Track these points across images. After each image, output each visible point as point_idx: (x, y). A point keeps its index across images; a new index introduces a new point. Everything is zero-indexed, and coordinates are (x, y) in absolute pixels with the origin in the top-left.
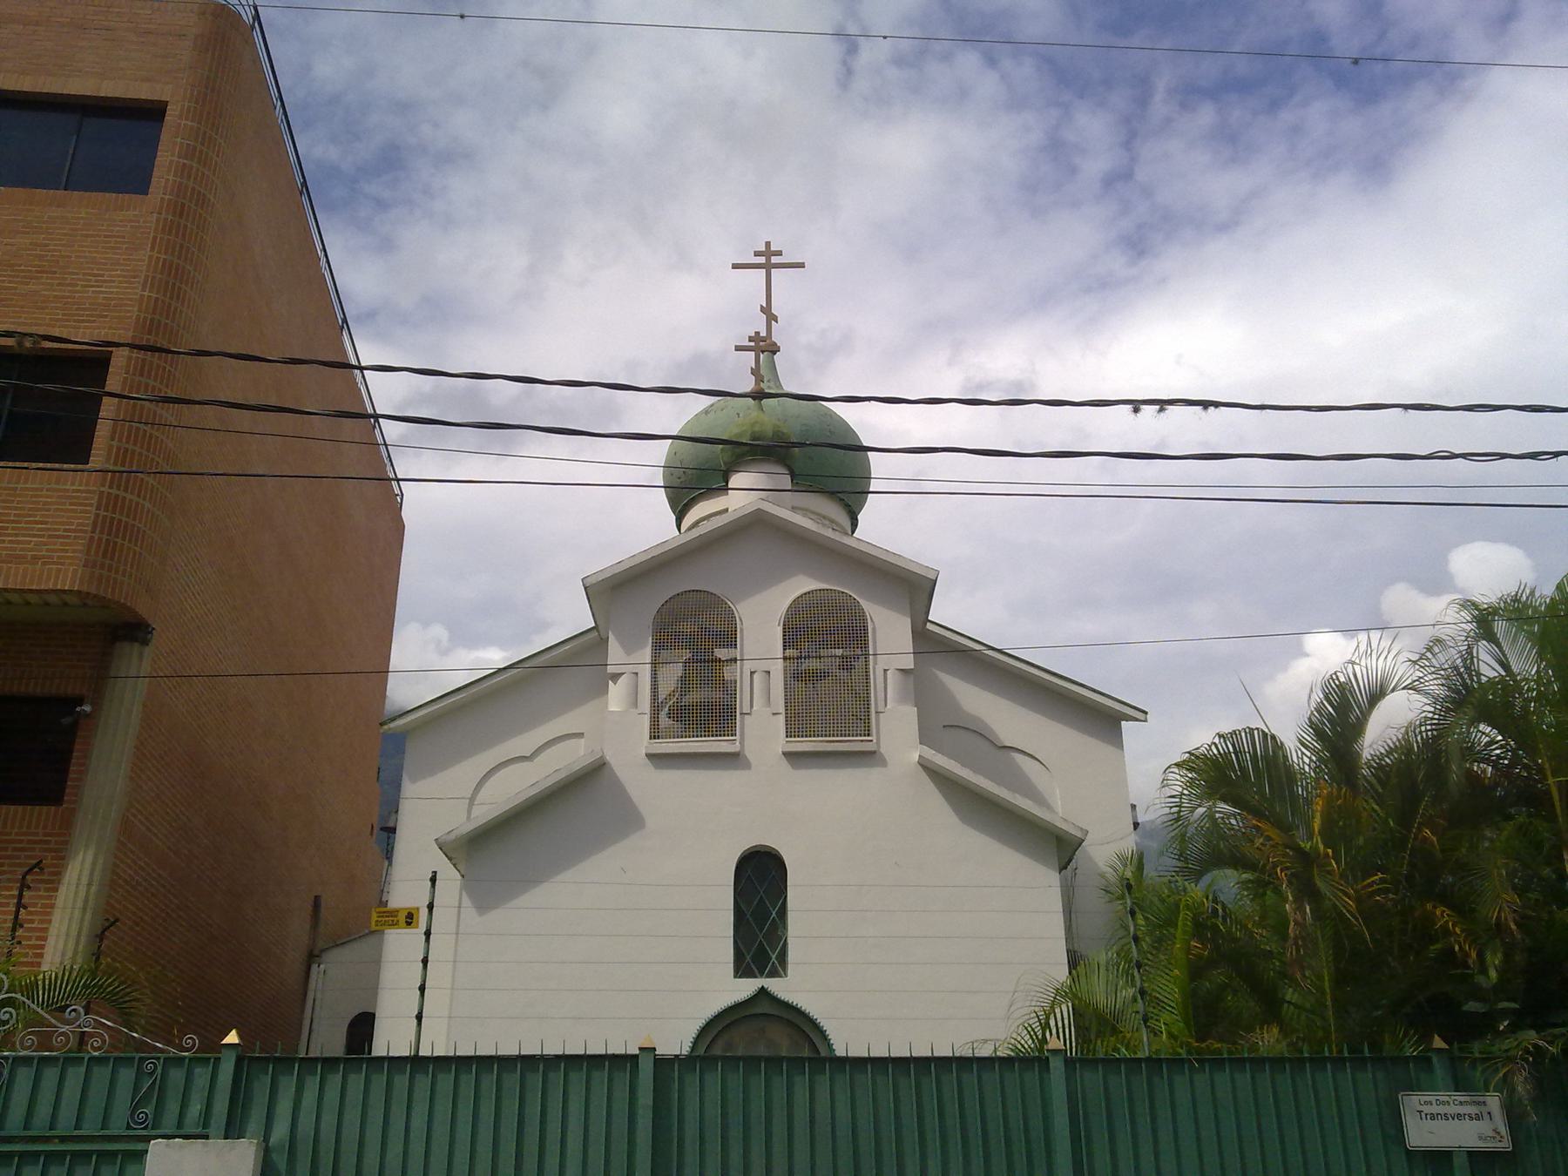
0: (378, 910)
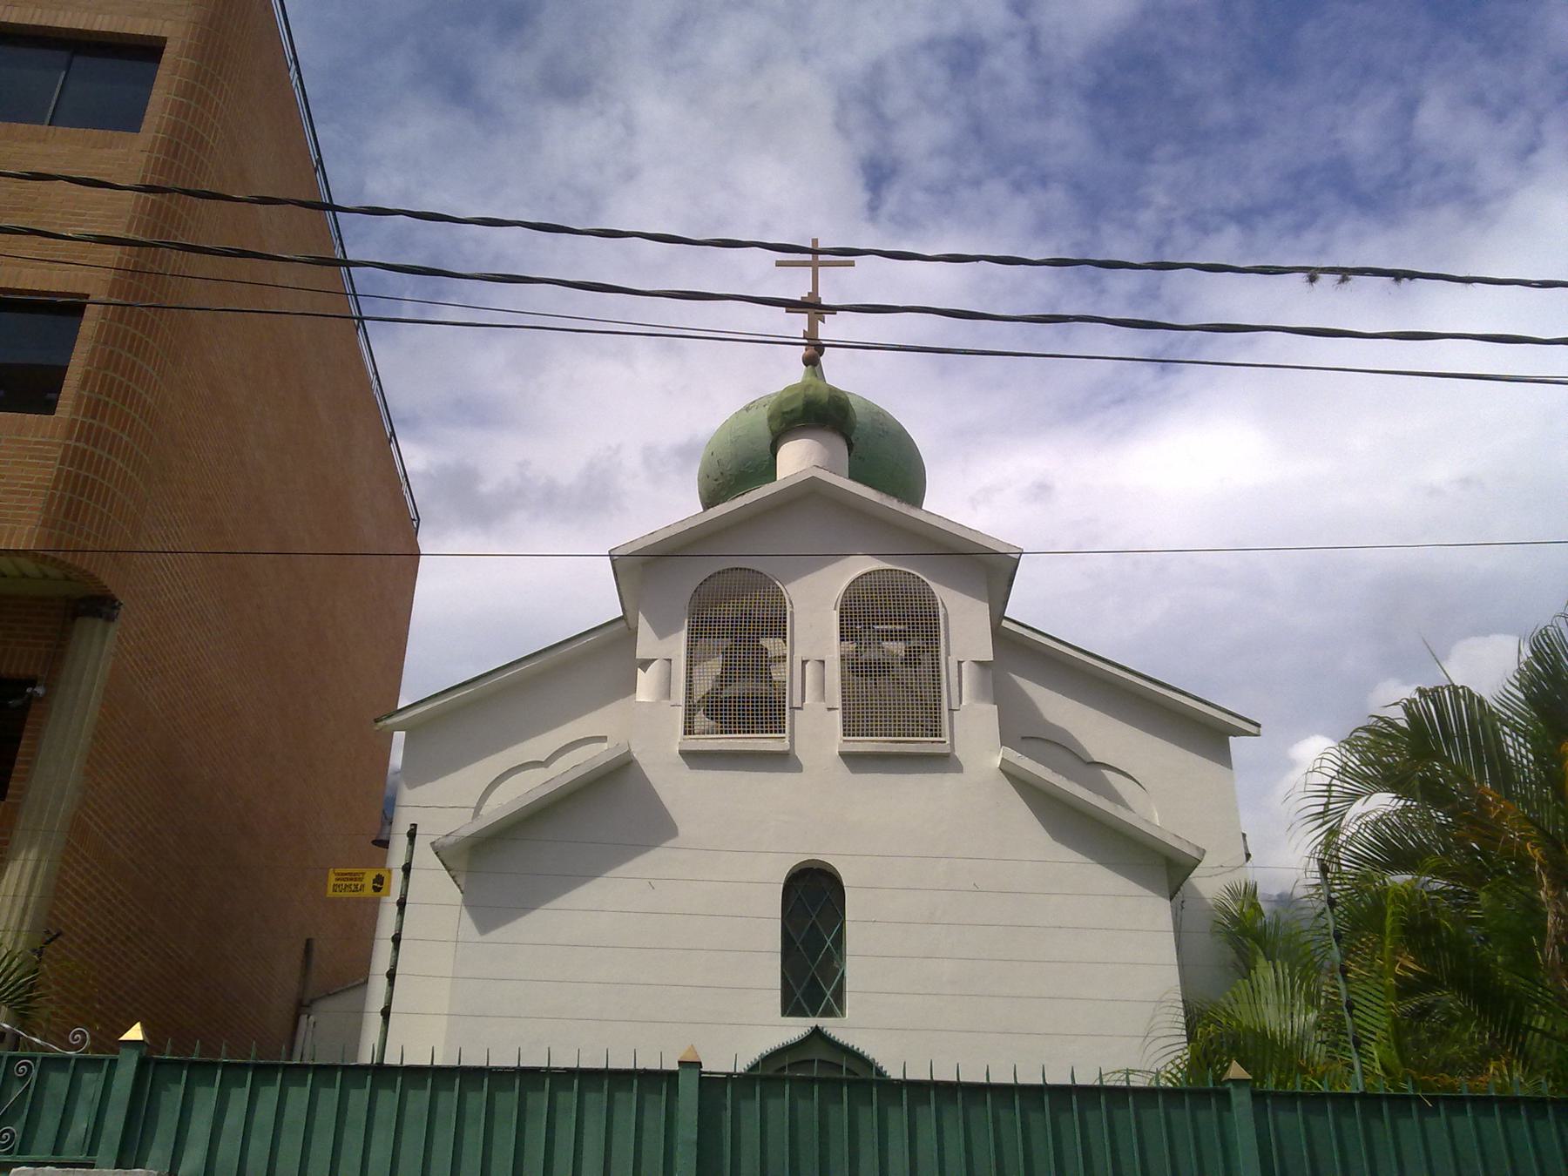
0: (337, 871)
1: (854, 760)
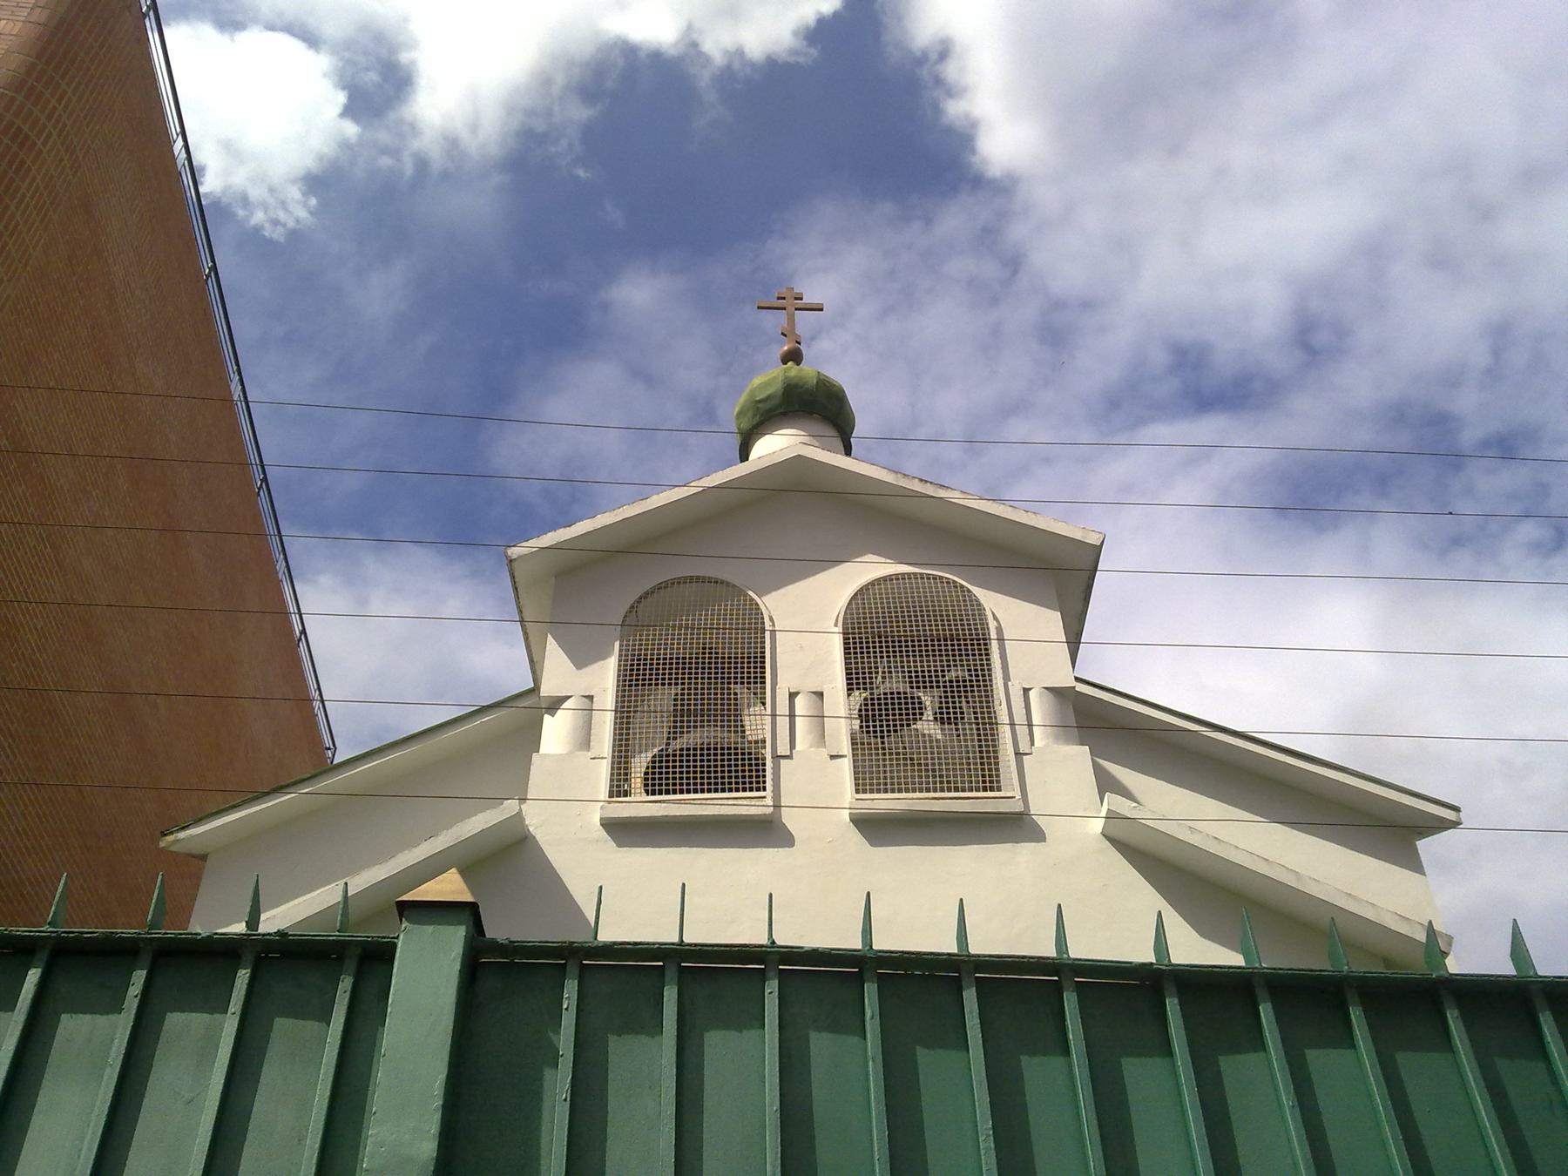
1: (874, 828)
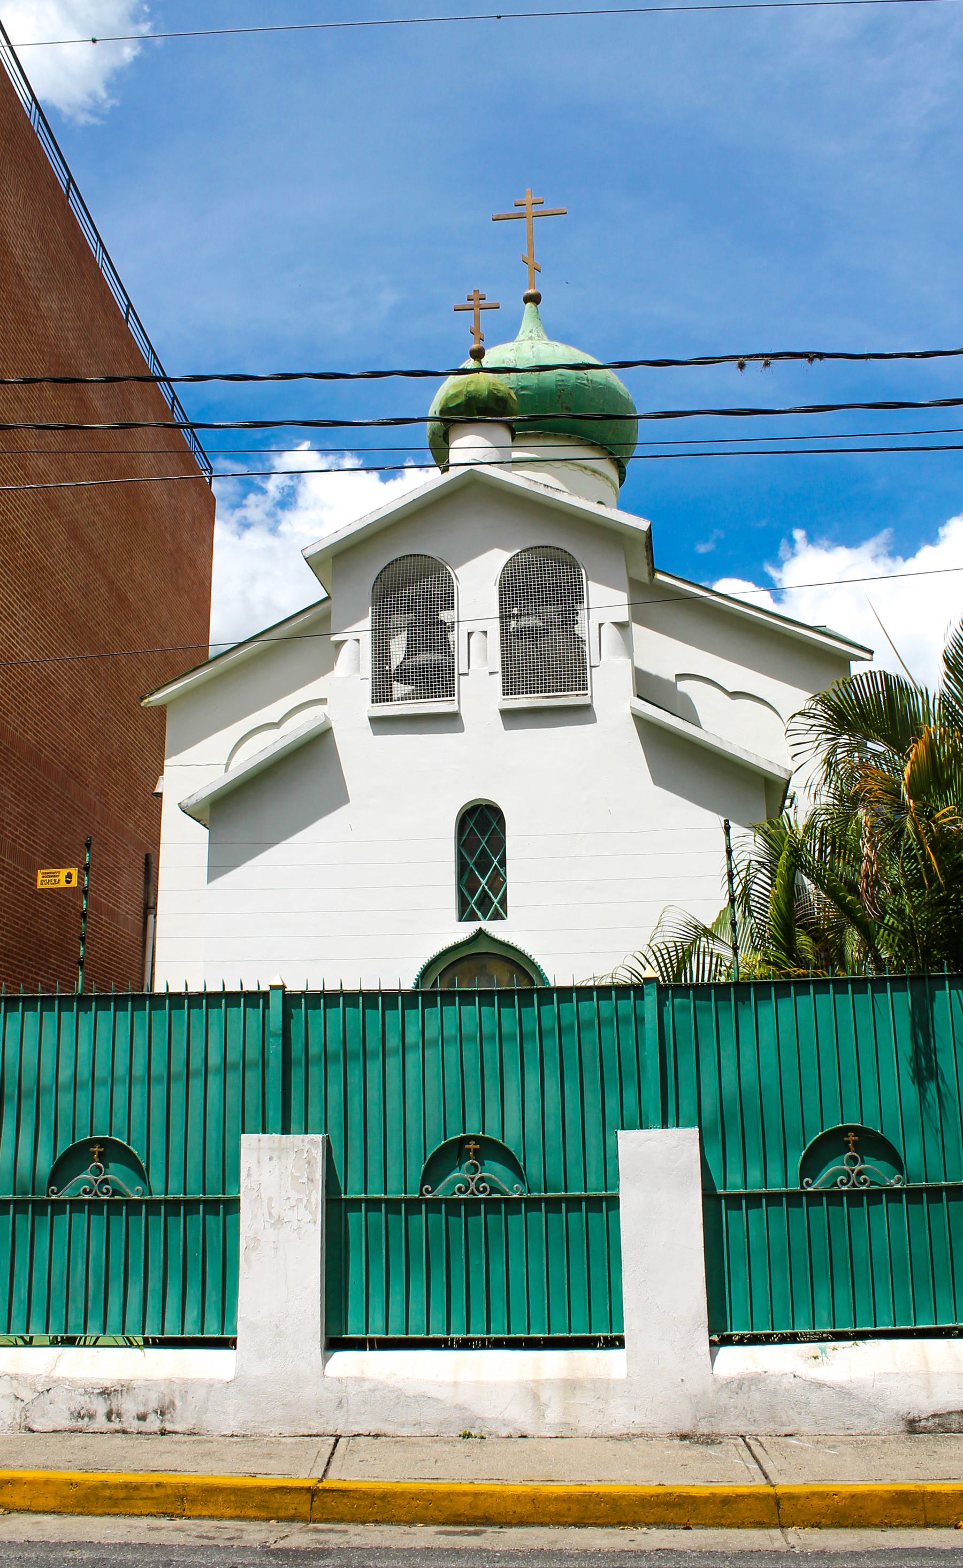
1: (511, 717)
